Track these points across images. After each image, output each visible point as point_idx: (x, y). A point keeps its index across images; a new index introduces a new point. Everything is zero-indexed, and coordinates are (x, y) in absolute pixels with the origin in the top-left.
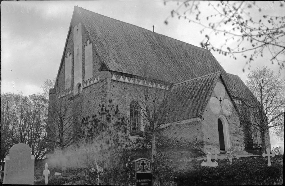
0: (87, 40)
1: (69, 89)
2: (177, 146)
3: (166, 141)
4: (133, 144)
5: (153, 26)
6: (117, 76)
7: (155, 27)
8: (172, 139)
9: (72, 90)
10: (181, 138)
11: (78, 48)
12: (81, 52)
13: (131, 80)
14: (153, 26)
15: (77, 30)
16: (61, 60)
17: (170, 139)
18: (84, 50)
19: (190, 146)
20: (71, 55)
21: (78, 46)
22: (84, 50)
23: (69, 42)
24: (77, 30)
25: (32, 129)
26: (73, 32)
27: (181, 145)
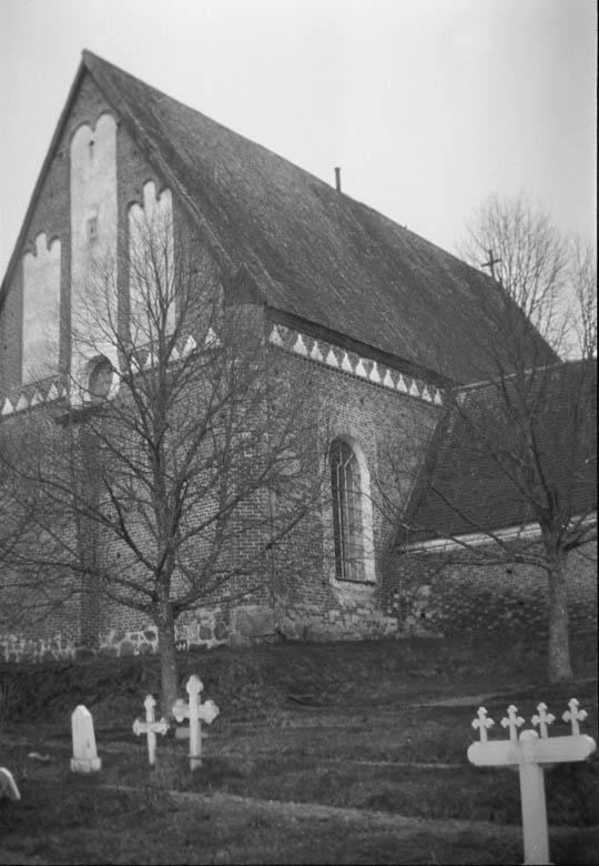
0: (145, 183)
1: (41, 385)
2: (517, 621)
3: (467, 604)
4: (342, 613)
5: (337, 170)
6: (287, 330)
7: (341, 173)
8: (494, 594)
9: (66, 385)
10: (536, 588)
11: (92, 214)
12: (108, 226)
13: (331, 354)
14: (337, 170)
15: (92, 143)
16: (7, 265)
17: (487, 596)
18: (123, 224)
19: (579, 618)
20: (57, 245)
21: (96, 207)
22: (123, 224)
23: (47, 188)
24: (92, 143)
25: (272, 520)
26: (68, 152)
27: (538, 618)
